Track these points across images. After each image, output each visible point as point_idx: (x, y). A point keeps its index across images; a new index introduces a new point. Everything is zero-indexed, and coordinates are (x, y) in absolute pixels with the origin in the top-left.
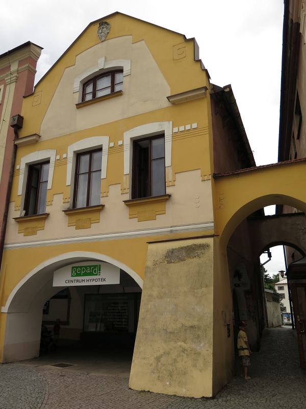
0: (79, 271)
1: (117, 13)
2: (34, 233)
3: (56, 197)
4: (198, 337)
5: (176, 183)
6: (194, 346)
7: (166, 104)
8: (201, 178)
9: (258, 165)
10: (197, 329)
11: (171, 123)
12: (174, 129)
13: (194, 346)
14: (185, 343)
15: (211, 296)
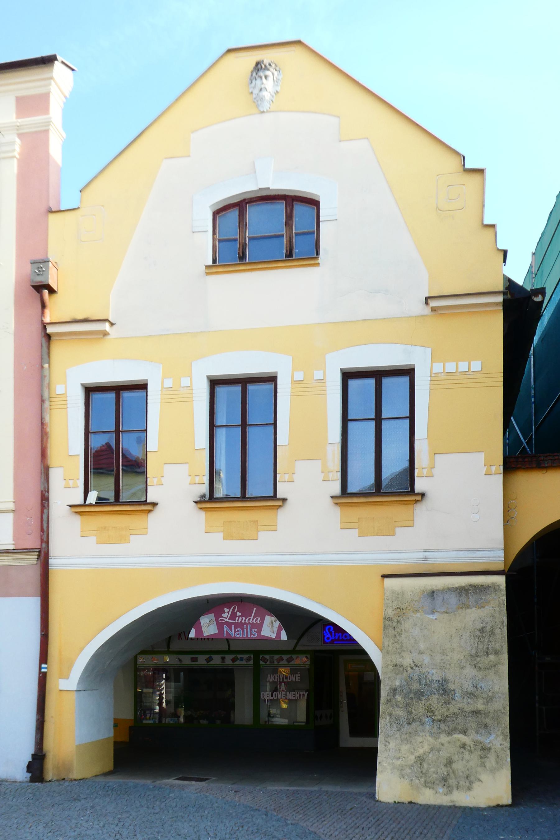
0: (238, 631)
1: (299, 43)
2: (123, 540)
3: (300, 466)
4: (486, 726)
5: (435, 471)
6: (479, 738)
7: (420, 309)
8: (64, 482)
9: (416, 492)
10: (483, 715)
11: (429, 351)
12: (435, 365)
13: (479, 738)
14: (465, 735)
15: (504, 669)
